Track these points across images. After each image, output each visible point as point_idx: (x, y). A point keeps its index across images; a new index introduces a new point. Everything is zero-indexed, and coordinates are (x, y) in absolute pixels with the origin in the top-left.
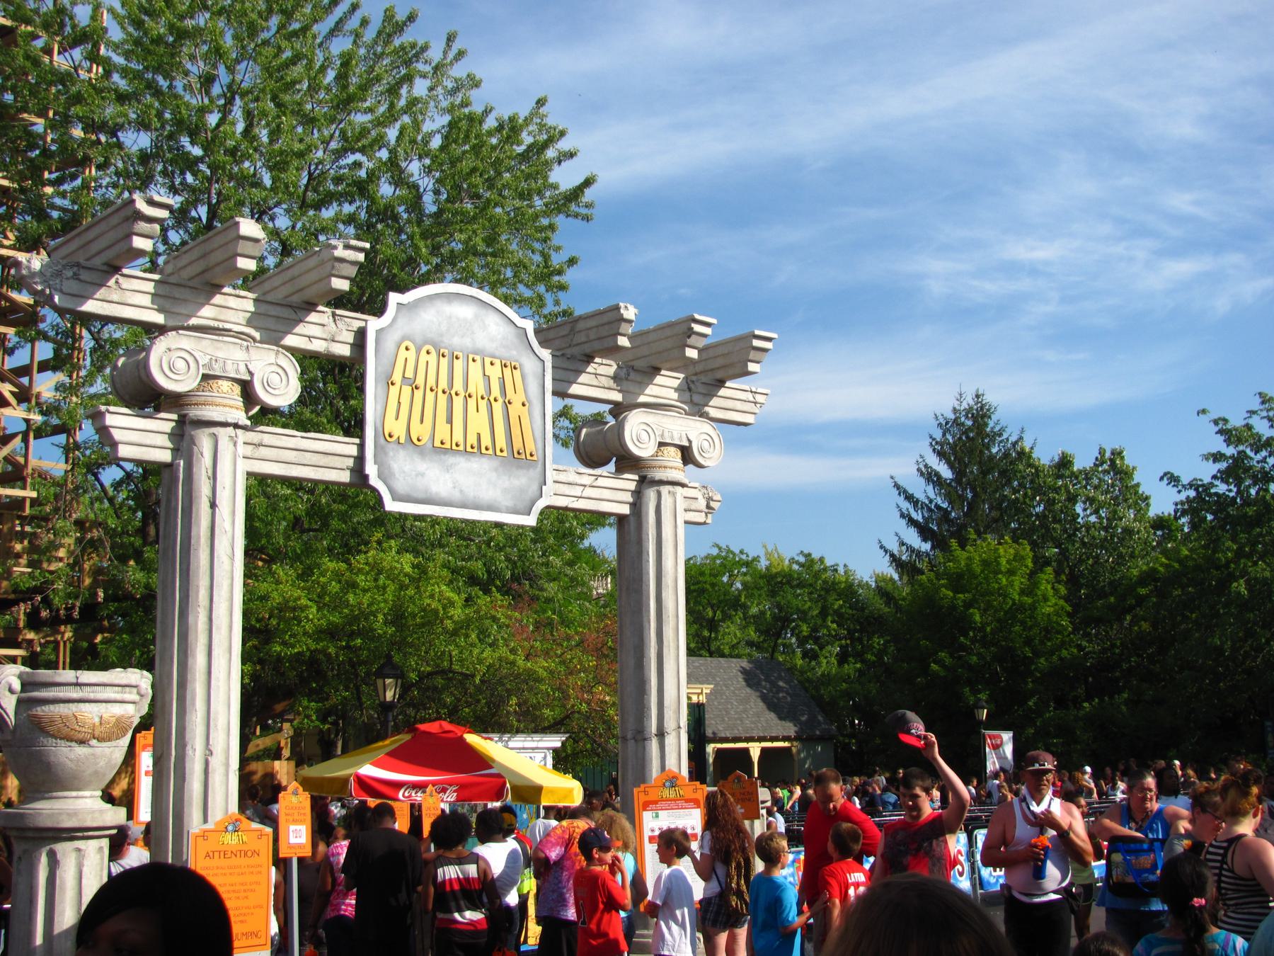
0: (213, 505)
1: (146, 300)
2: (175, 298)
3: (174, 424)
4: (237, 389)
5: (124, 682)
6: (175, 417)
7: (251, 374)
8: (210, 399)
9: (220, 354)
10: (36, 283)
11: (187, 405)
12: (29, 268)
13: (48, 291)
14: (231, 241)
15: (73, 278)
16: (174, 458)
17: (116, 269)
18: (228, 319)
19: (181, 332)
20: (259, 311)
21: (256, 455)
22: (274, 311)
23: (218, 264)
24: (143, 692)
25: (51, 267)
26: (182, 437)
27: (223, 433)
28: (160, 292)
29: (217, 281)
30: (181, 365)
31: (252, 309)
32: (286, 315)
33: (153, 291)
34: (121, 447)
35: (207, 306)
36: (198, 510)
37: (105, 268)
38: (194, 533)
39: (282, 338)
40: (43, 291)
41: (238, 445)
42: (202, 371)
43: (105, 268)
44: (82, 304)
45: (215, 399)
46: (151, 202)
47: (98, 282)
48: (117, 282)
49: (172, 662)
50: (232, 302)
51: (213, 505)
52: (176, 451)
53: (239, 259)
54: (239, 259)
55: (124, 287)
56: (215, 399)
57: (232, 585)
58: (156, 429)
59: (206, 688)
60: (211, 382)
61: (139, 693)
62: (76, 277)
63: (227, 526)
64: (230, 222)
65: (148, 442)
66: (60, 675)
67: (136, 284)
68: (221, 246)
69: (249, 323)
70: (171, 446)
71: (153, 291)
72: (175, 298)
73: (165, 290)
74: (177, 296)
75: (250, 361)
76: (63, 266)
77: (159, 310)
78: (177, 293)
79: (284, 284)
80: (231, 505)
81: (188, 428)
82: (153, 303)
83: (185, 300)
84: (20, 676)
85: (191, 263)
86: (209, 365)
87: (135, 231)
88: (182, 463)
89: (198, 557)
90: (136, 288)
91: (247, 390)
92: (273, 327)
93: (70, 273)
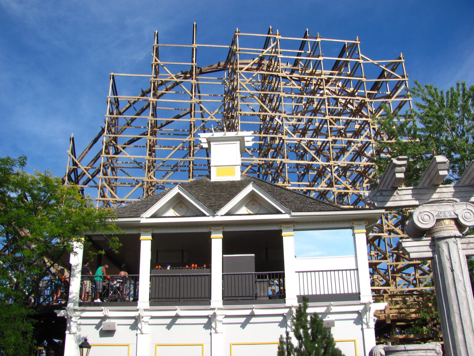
0: (452, 271)
1: (410, 197)
2: (421, 194)
3: (430, 241)
4: (453, 223)
5: (426, 348)
6: (430, 238)
7: (457, 215)
8: (442, 228)
9: (442, 210)
10: (368, 201)
11: (434, 233)
12: (364, 196)
13: (372, 202)
14: (435, 166)
15: (380, 195)
16: (433, 254)
17: (396, 189)
18: (445, 197)
19: (423, 205)
20: (456, 191)
21: (468, 248)
22: (463, 189)
23: (434, 177)
24: (438, 352)
25: (372, 194)
26: (434, 246)
27: (450, 241)
28: (414, 193)
29: (436, 183)
30: (426, 217)
31: (454, 191)
32: (469, 190)
33: (412, 193)
34: (411, 254)
35: (435, 194)
36: (446, 274)
37: (391, 189)
38: (446, 283)
39: (469, 199)
40: (371, 203)
41: (458, 244)
42: (435, 218)
43: (391, 189)
44: (386, 205)
45: (444, 228)
46: (399, 160)
47: (390, 195)
48: (397, 193)
49: (448, 338)
50: (444, 190)
51: (452, 271)
52: (433, 252)
53: (440, 172)
54: (440, 172)
55: (400, 194)
56: (444, 228)
57: (468, 303)
58: (423, 245)
59: (465, 348)
60: (441, 222)
61: (436, 352)
62: (381, 195)
63: (461, 278)
64: (433, 159)
65: (421, 250)
66: (398, 347)
67: (404, 192)
68: (433, 169)
69: (454, 196)
70: (431, 250)
71: (411, 193)
72: (421, 194)
73: (415, 192)
74: (421, 193)
75: (455, 210)
76: (376, 192)
77: (416, 200)
78: (421, 191)
79: (466, 179)
80: (461, 269)
81: (436, 242)
82: (413, 197)
83: (425, 194)
84: (384, 349)
85: (426, 180)
86: (438, 215)
87: (396, 171)
88: (436, 256)
89: (450, 292)
90: (405, 193)
91: (456, 221)
92: (464, 196)
93: (379, 194)
